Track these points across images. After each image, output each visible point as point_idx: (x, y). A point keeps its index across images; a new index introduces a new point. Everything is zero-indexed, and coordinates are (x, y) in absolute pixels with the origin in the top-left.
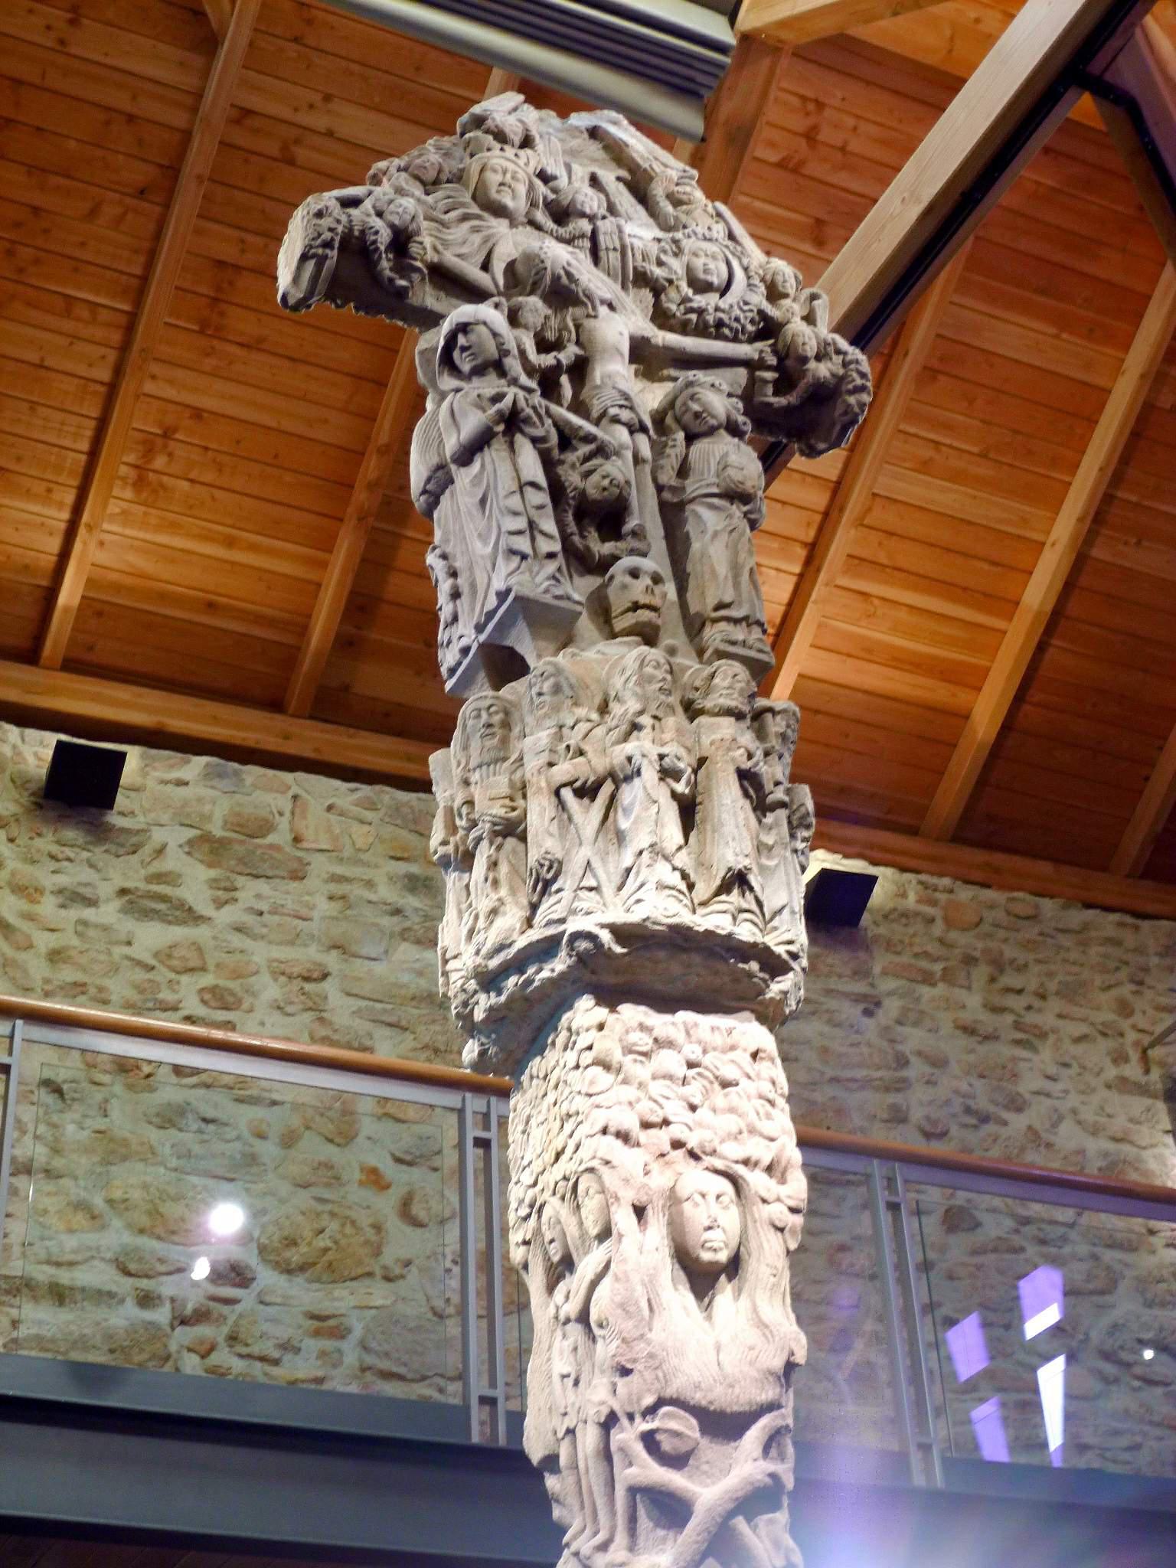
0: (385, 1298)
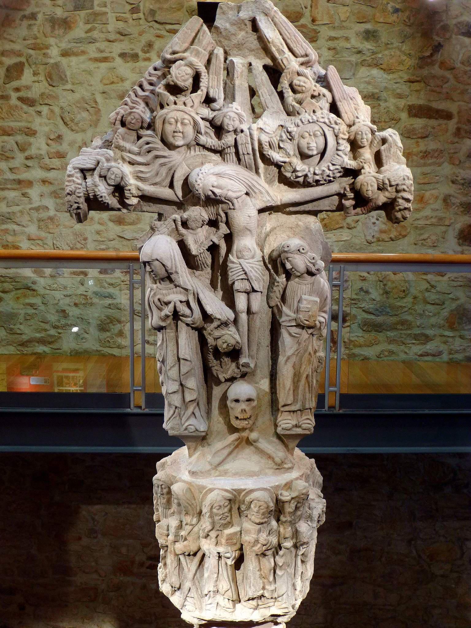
0: (348, 237)
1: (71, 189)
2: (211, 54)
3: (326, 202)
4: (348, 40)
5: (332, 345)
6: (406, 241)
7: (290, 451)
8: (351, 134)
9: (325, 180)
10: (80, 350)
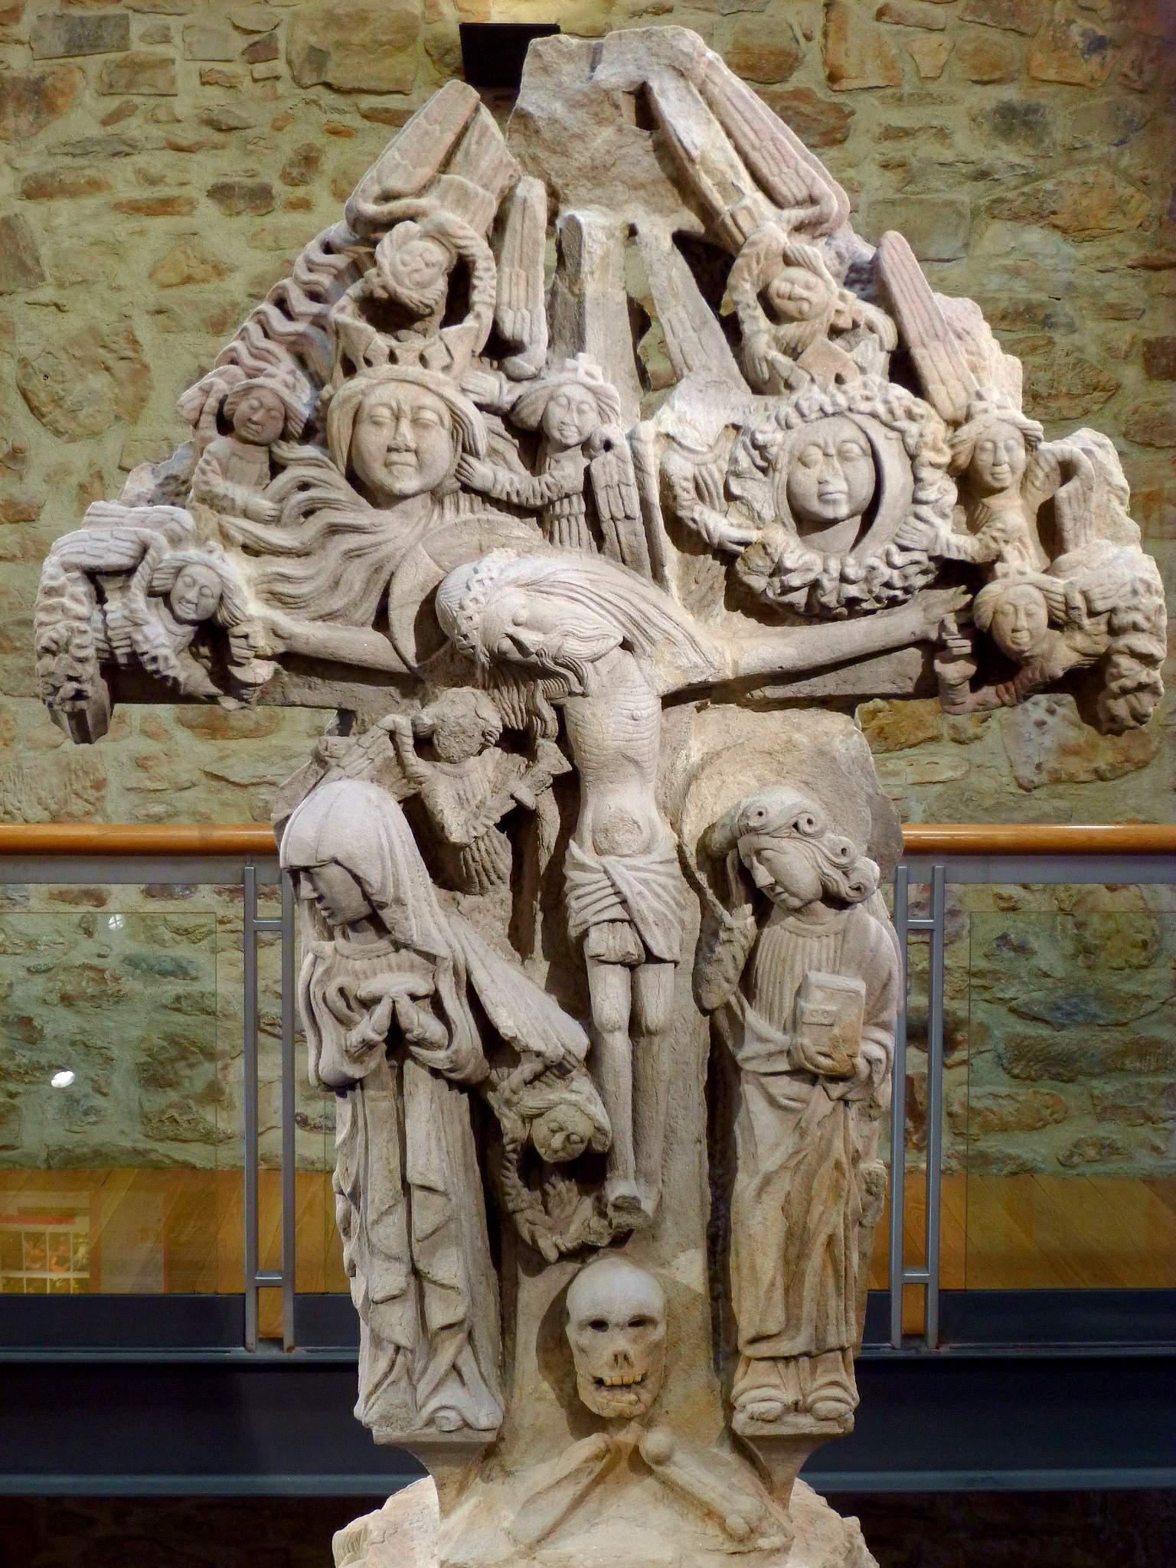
0: (954, 768)
1: (55, 636)
2: (506, 199)
5: (910, 1124)
6: (1145, 780)
7: (775, 1489)
8: (960, 448)
9: (878, 599)
10: (79, 1151)
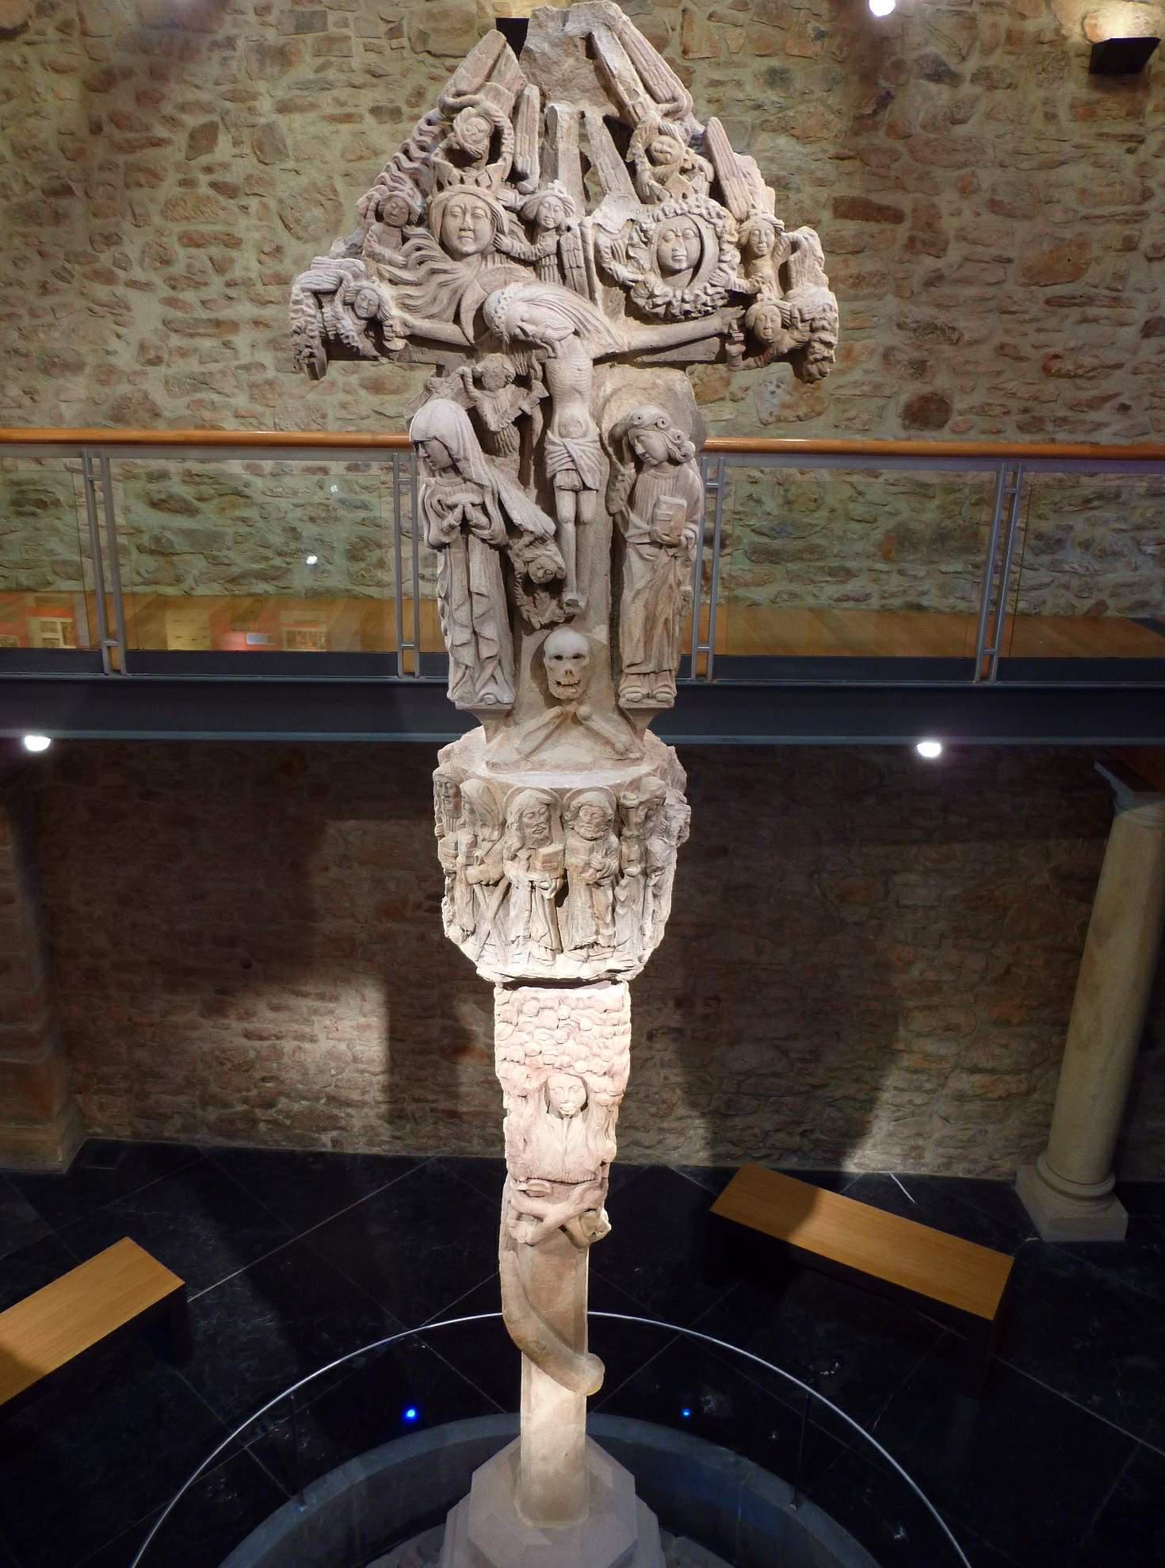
2: (519, 96)
3: (700, 347)
4: (740, 85)
7: (638, 733)
9: (700, 312)
